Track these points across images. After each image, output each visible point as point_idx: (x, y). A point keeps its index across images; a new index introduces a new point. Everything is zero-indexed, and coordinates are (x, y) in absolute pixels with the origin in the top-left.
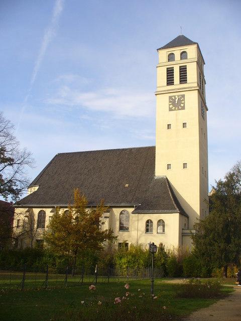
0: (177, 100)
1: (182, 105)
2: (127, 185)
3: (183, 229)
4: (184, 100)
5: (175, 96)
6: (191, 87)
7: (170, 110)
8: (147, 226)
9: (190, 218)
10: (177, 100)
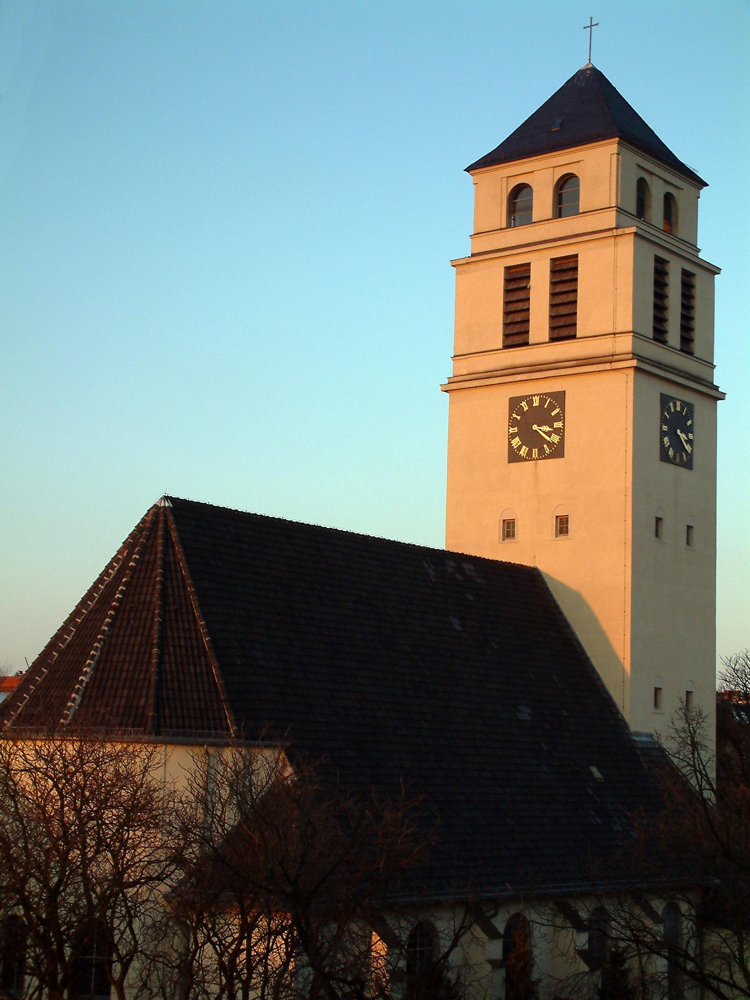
7: (514, 457)
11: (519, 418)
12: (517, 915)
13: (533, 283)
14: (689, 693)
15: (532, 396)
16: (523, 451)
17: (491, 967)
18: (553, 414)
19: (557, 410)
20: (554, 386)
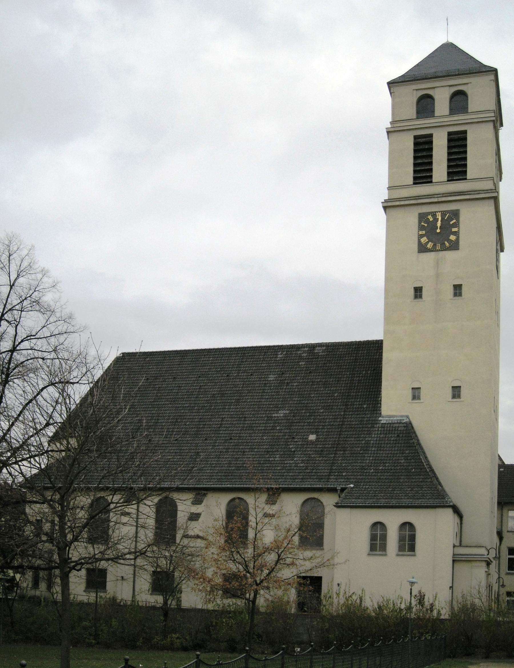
0: (439, 224)
1: (453, 238)
2: (312, 437)
3: (454, 546)
4: (456, 225)
5: (434, 214)
6: (479, 192)
7: (422, 249)
8: (413, 538)
9: (464, 518)
10: (439, 224)
11: (426, 225)
12: (166, 497)
13: (435, 167)
14: (436, 595)
15: (436, 212)
16: (430, 245)
17: (506, 463)
18: (451, 223)
19: (454, 221)
20: (456, 118)
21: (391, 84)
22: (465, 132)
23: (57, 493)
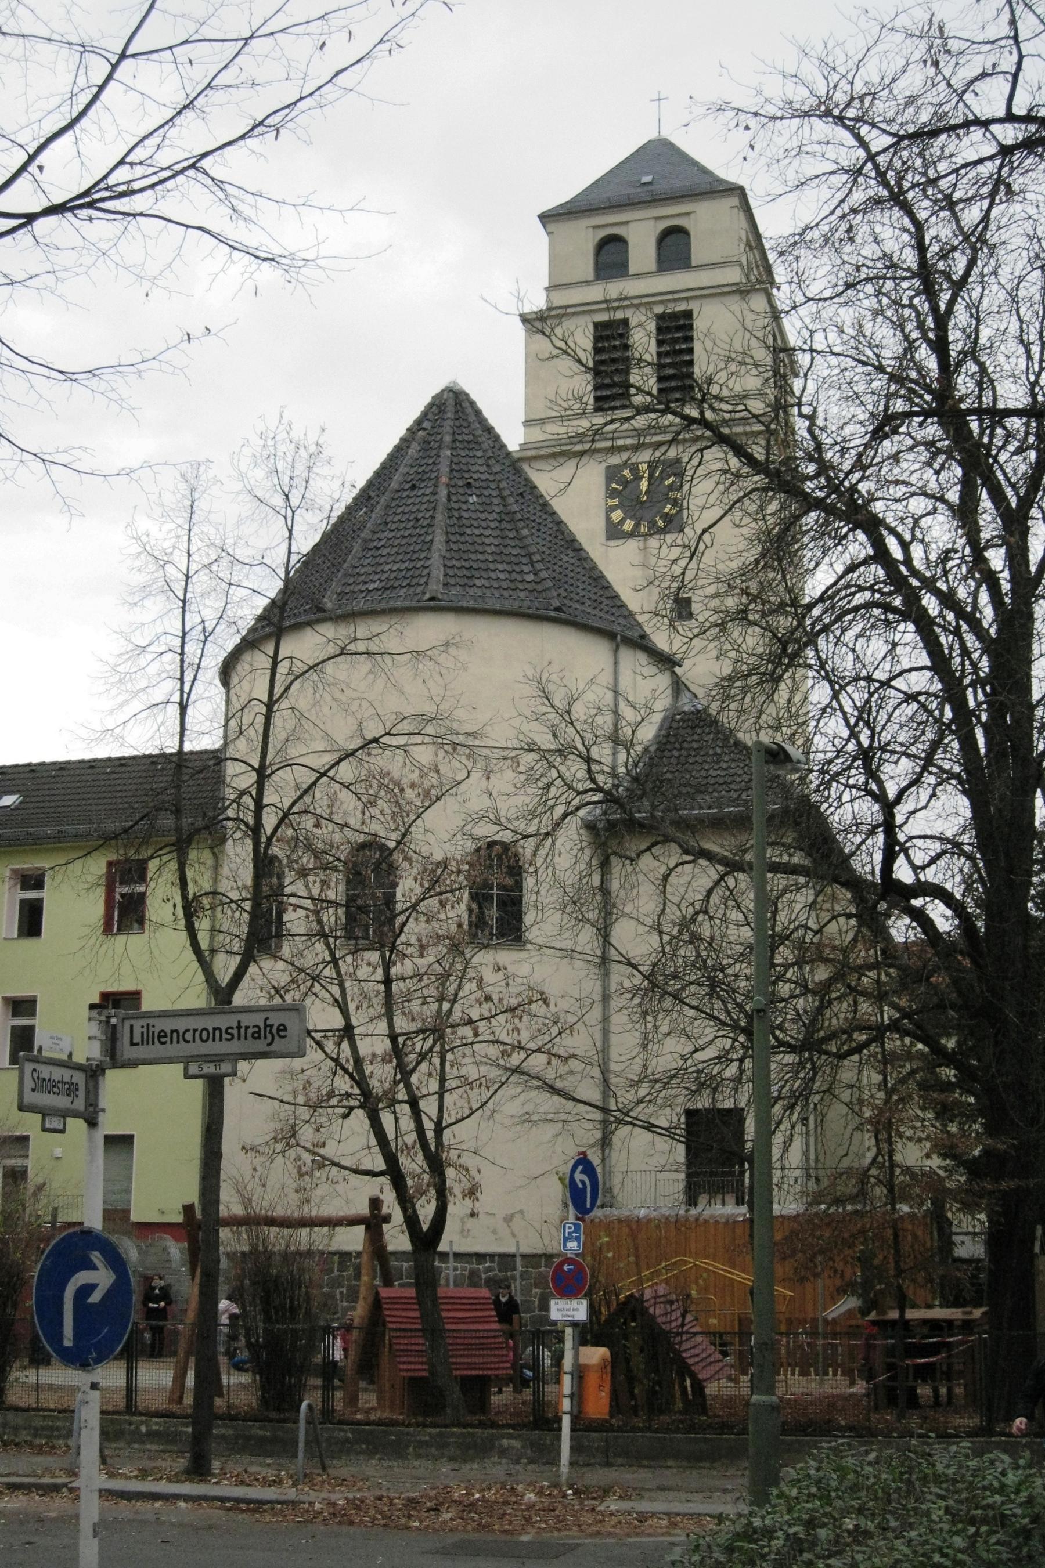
16: (628, 525)
21: (546, 218)
22: (688, 315)
23: (938, 1070)
